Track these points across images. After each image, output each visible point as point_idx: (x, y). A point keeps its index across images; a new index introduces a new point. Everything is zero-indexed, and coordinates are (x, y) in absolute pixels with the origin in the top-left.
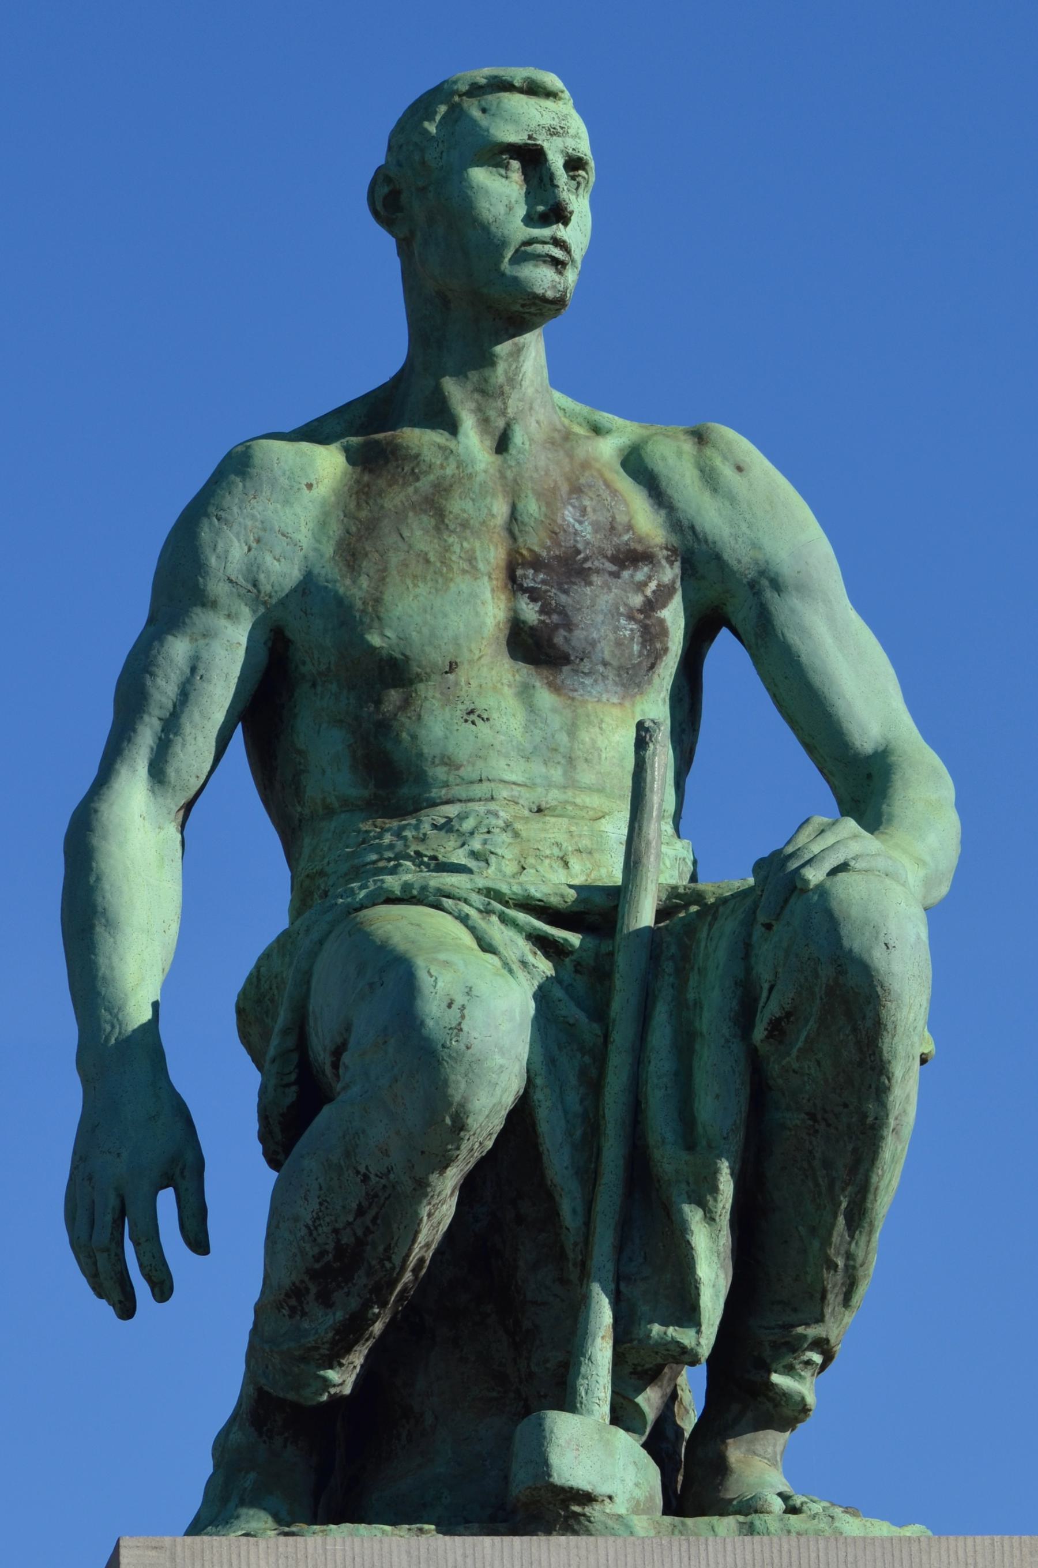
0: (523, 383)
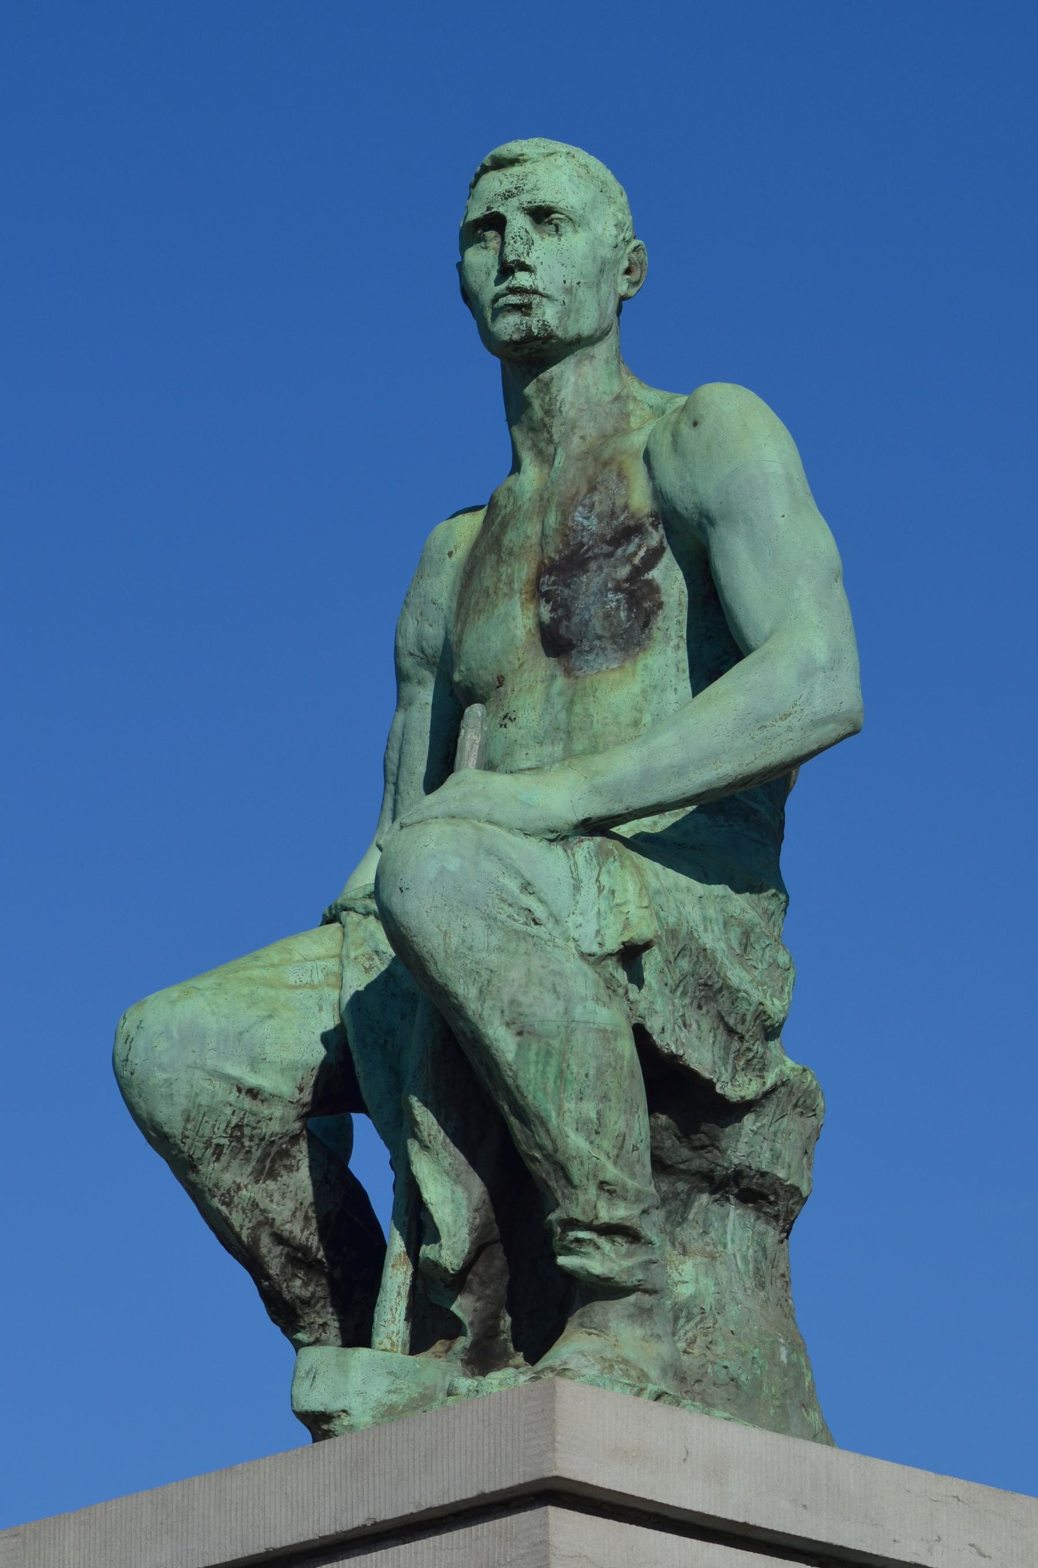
0: (563, 409)
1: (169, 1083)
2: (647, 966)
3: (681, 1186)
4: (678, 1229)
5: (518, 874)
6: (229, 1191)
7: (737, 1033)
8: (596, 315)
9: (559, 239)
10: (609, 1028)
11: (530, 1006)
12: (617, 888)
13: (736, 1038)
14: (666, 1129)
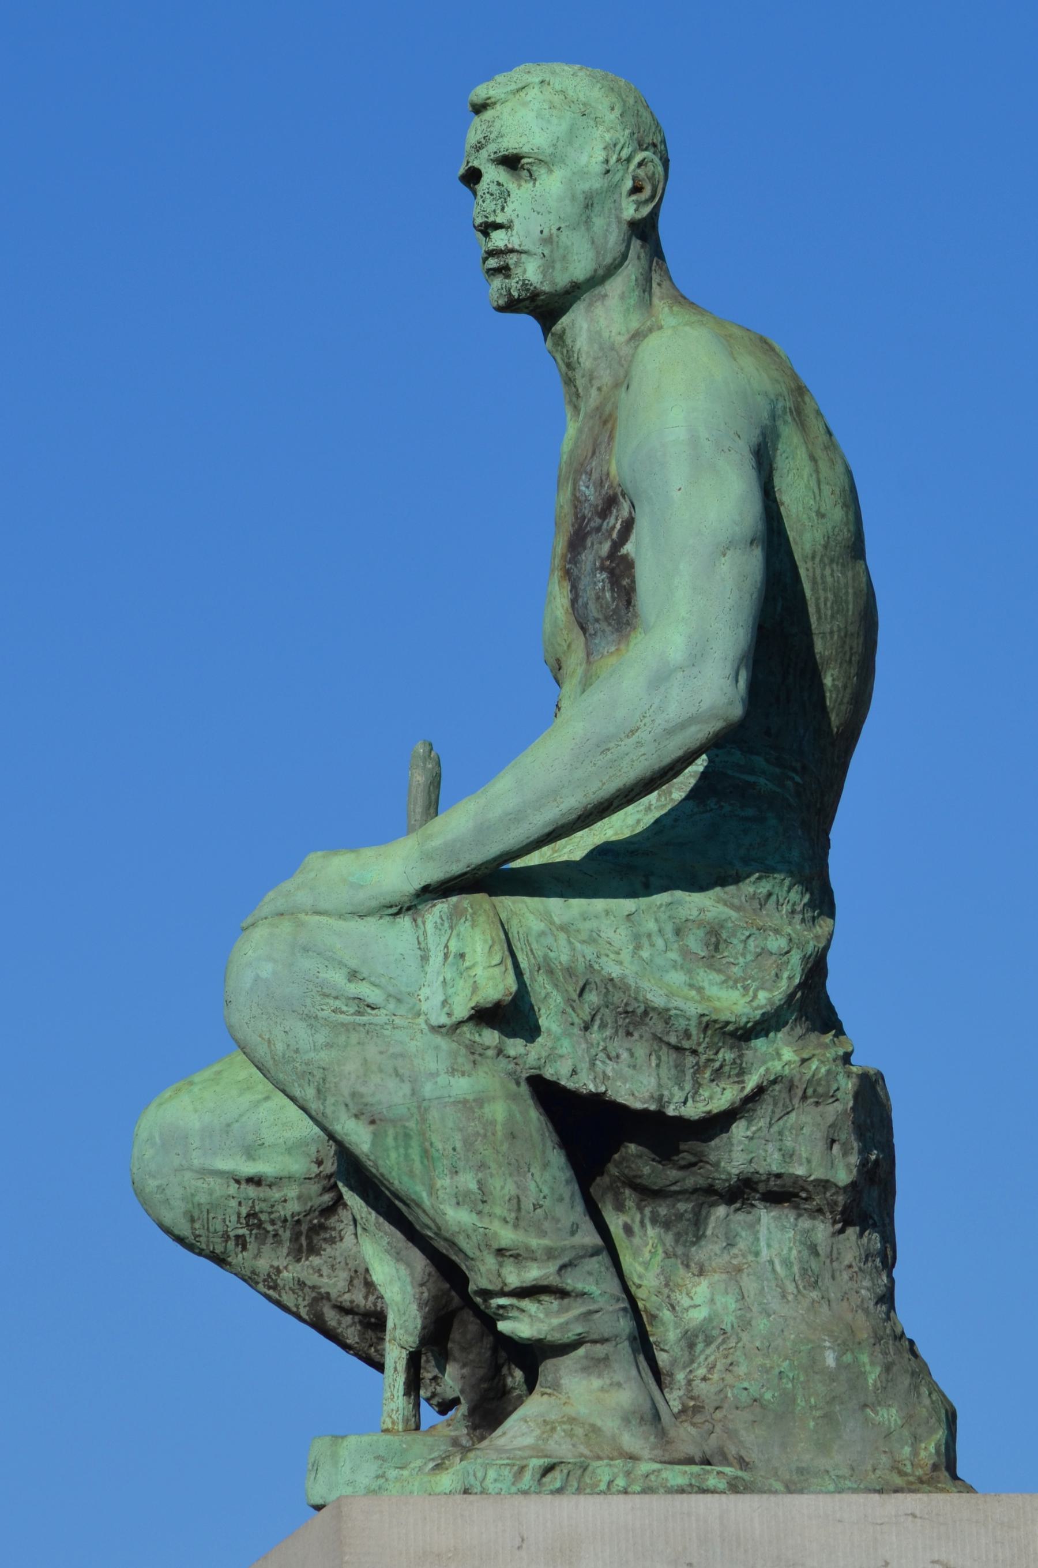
0: (581, 360)
1: (161, 1189)
2: (543, 1011)
3: (682, 1206)
4: (693, 1249)
5: (341, 964)
6: (269, 1275)
7: (686, 1049)
8: (591, 254)
9: (534, 186)
10: (470, 1097)
11: (373, 1095)
12: (467, 950)
13: (687, 1053)
14: (640, 1156)
